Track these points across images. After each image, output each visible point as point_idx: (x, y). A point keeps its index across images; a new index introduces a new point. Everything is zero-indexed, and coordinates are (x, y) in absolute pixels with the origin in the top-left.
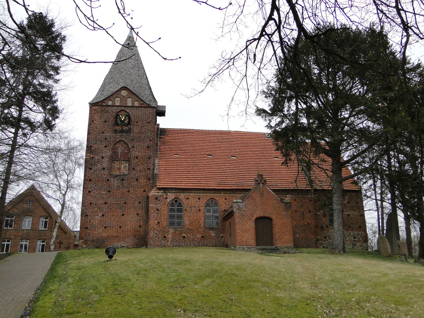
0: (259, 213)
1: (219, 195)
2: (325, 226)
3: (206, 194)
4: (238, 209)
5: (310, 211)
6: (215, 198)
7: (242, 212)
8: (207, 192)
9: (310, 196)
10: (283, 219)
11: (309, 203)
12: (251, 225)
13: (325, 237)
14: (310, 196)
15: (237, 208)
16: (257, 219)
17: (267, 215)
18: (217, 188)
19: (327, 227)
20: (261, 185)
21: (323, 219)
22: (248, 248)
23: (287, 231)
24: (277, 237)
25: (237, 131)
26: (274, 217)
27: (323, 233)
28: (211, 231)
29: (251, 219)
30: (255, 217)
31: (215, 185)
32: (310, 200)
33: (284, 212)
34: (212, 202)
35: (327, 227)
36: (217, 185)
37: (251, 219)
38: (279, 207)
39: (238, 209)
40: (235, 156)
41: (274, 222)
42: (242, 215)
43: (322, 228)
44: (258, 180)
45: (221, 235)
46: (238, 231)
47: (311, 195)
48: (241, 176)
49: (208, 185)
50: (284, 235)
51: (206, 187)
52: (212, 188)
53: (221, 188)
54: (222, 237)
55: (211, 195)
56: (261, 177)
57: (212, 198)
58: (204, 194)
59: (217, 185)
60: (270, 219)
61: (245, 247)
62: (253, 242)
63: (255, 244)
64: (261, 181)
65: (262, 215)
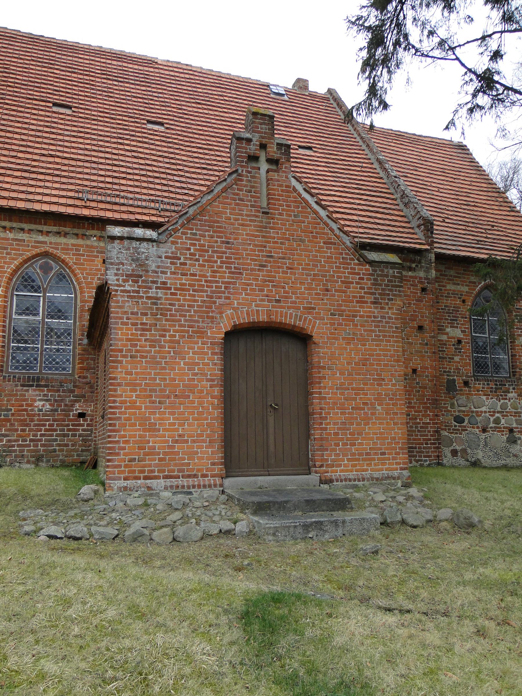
0: (248, 306)
1: (80, 242)
2: (459, 381)
3: (21, 236)
4: (134, 277)
5: (420, 328)
6: (58, 253)
7: (152, 293)
8: (26, 226)
9: (422, 274)
10: (363, 341)
11: (419, 300)
12: (200, 364)
13: (459, 420)
14: (422, 274)
15: (129, 268)
16: (235, 334)
17: (288, 316)
18: (70, 211)
19: (466, 383)
20: (264, 166)
21: (457, 359)
22: (176, 490)
23: (379, 399)
24: (332, 428)
25: (179, 63)
26: (318, 328)
27: (452, 405)
28: (31, 392)
29: (201, 333)
30: (225, 326)
31: (63, 201)
32: (424, 290)
33: (369, 309)
34: (46, 269)
35: (466, 383)
36: (70, 202)
37: (201, 333)
38: (347, 283)
39: (134, 277)
40: (162, 124)
41: (323, 352)
42: (157, 309)
43: (451, 386)
44: (249, 140)
45: (78, 408)
46: (123, 394)
47: (427, 270)
48: (178, 185)
49: (30, 197)
50: (366, 420)
51: (21, 205)
52: (46, 208)
53: (86, 212)
54: (82, 415)
55: (41, 238)
56: (264, 128)
57: (46, 254)
58: (11, 235)
59: (70, 202)
60: (302, 338)
61: (158, 484)
62: (207, 455)
63: (218, 469)
64: (263, 146)
65: (263, 318)
